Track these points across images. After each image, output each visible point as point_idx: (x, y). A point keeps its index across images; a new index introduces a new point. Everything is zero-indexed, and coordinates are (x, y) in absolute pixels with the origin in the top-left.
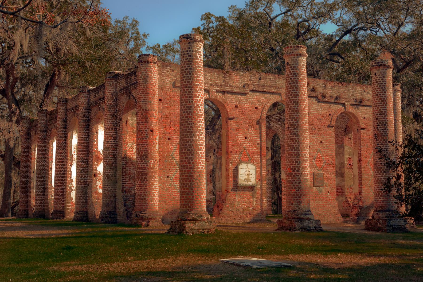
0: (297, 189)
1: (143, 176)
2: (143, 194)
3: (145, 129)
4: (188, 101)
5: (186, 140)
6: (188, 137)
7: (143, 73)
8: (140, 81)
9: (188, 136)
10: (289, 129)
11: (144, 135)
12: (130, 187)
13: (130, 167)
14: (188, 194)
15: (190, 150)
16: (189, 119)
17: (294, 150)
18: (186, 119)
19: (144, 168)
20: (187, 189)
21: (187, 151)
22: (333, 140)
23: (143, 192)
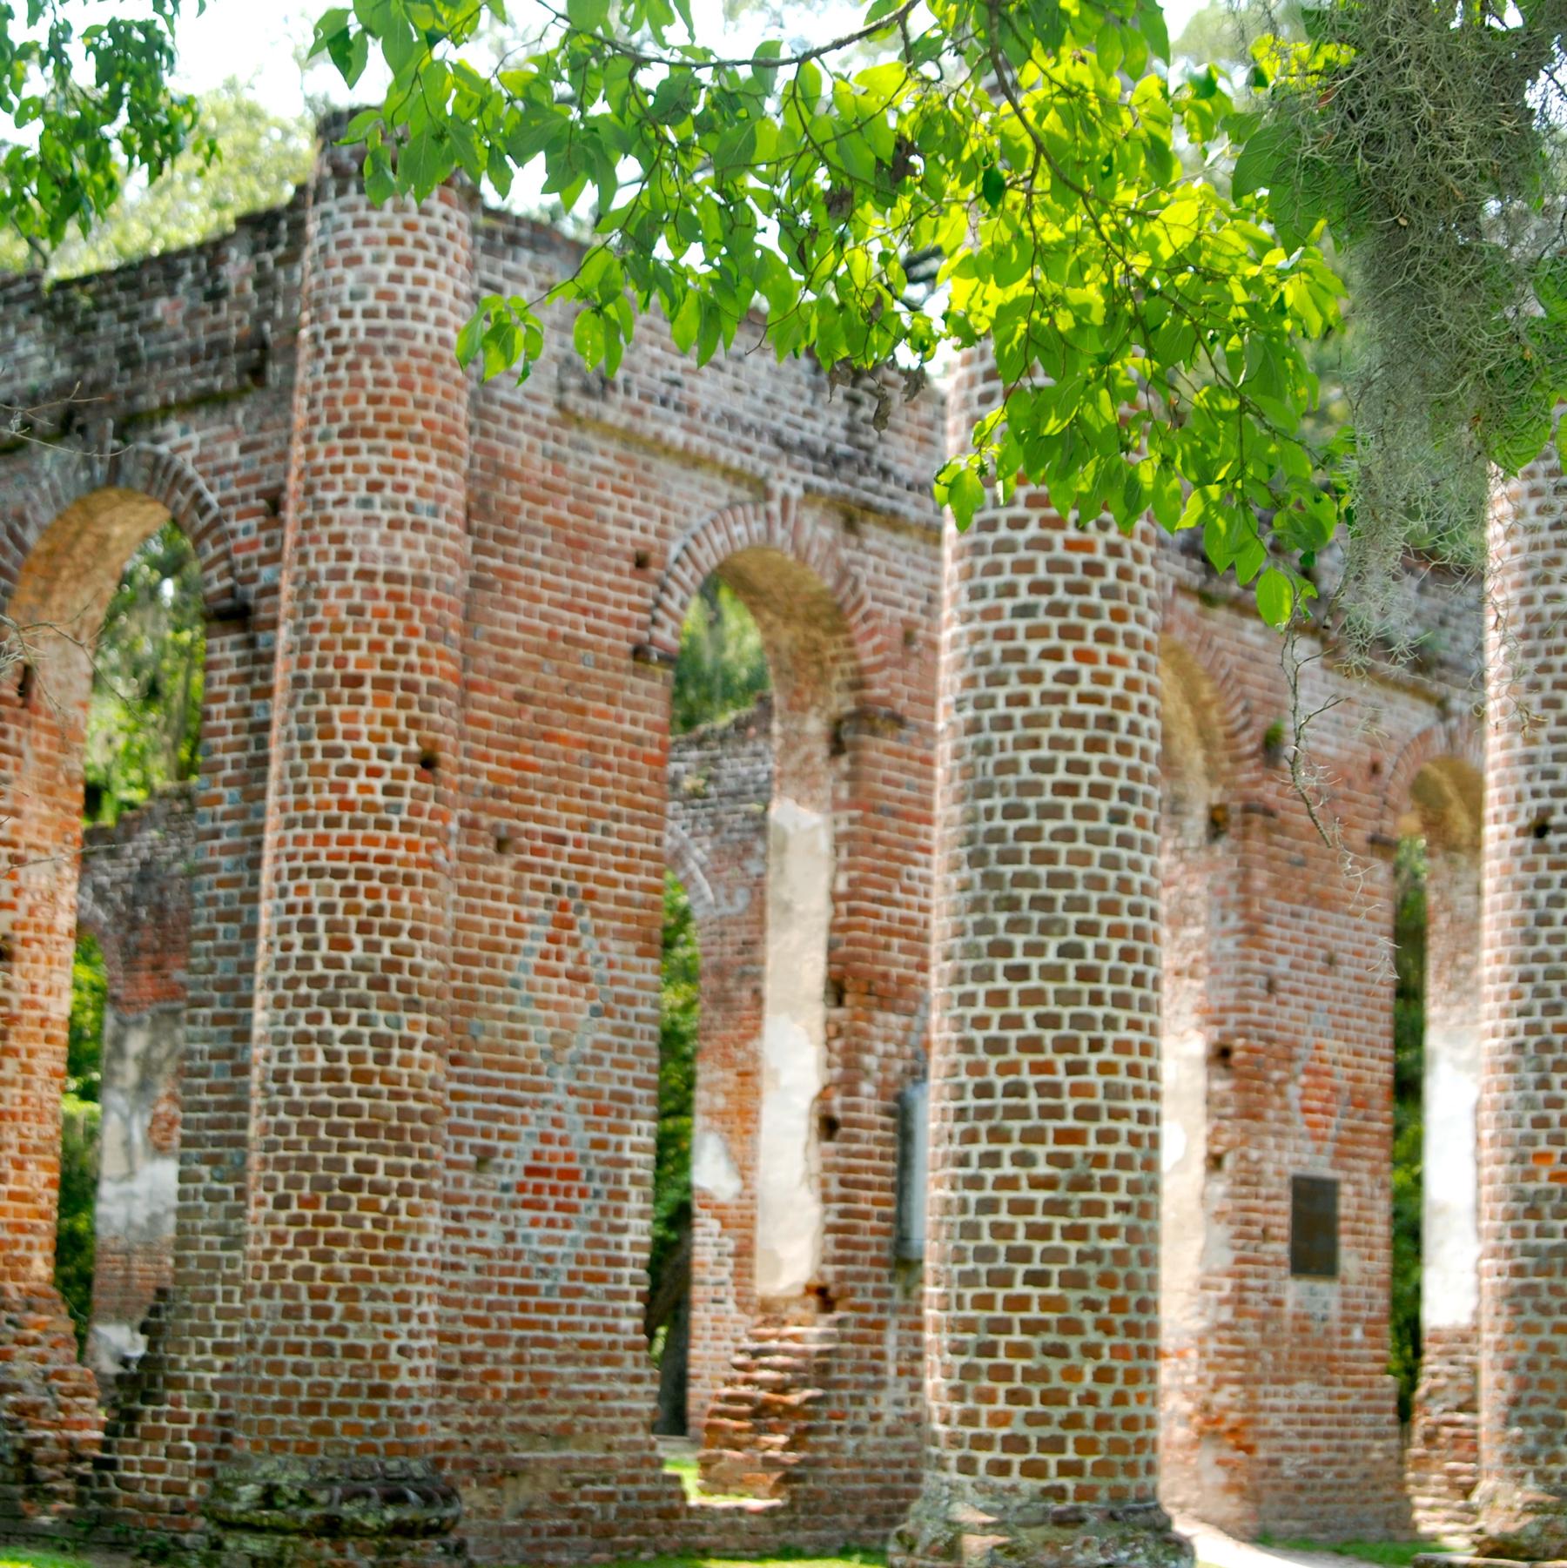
1: (343, 1147)
2: (339, 1308)
3: (374, 737)
7: (378, 259)
8: (345, 325)
11: (364, 789)
12: (20, 1228)
13: (31, 1054)
14: (1059, 1351)
16: (1071, 677)
18: (1050, 668)
19: (358, 1076)
21: (1051, 957)
23: (334, 1286)
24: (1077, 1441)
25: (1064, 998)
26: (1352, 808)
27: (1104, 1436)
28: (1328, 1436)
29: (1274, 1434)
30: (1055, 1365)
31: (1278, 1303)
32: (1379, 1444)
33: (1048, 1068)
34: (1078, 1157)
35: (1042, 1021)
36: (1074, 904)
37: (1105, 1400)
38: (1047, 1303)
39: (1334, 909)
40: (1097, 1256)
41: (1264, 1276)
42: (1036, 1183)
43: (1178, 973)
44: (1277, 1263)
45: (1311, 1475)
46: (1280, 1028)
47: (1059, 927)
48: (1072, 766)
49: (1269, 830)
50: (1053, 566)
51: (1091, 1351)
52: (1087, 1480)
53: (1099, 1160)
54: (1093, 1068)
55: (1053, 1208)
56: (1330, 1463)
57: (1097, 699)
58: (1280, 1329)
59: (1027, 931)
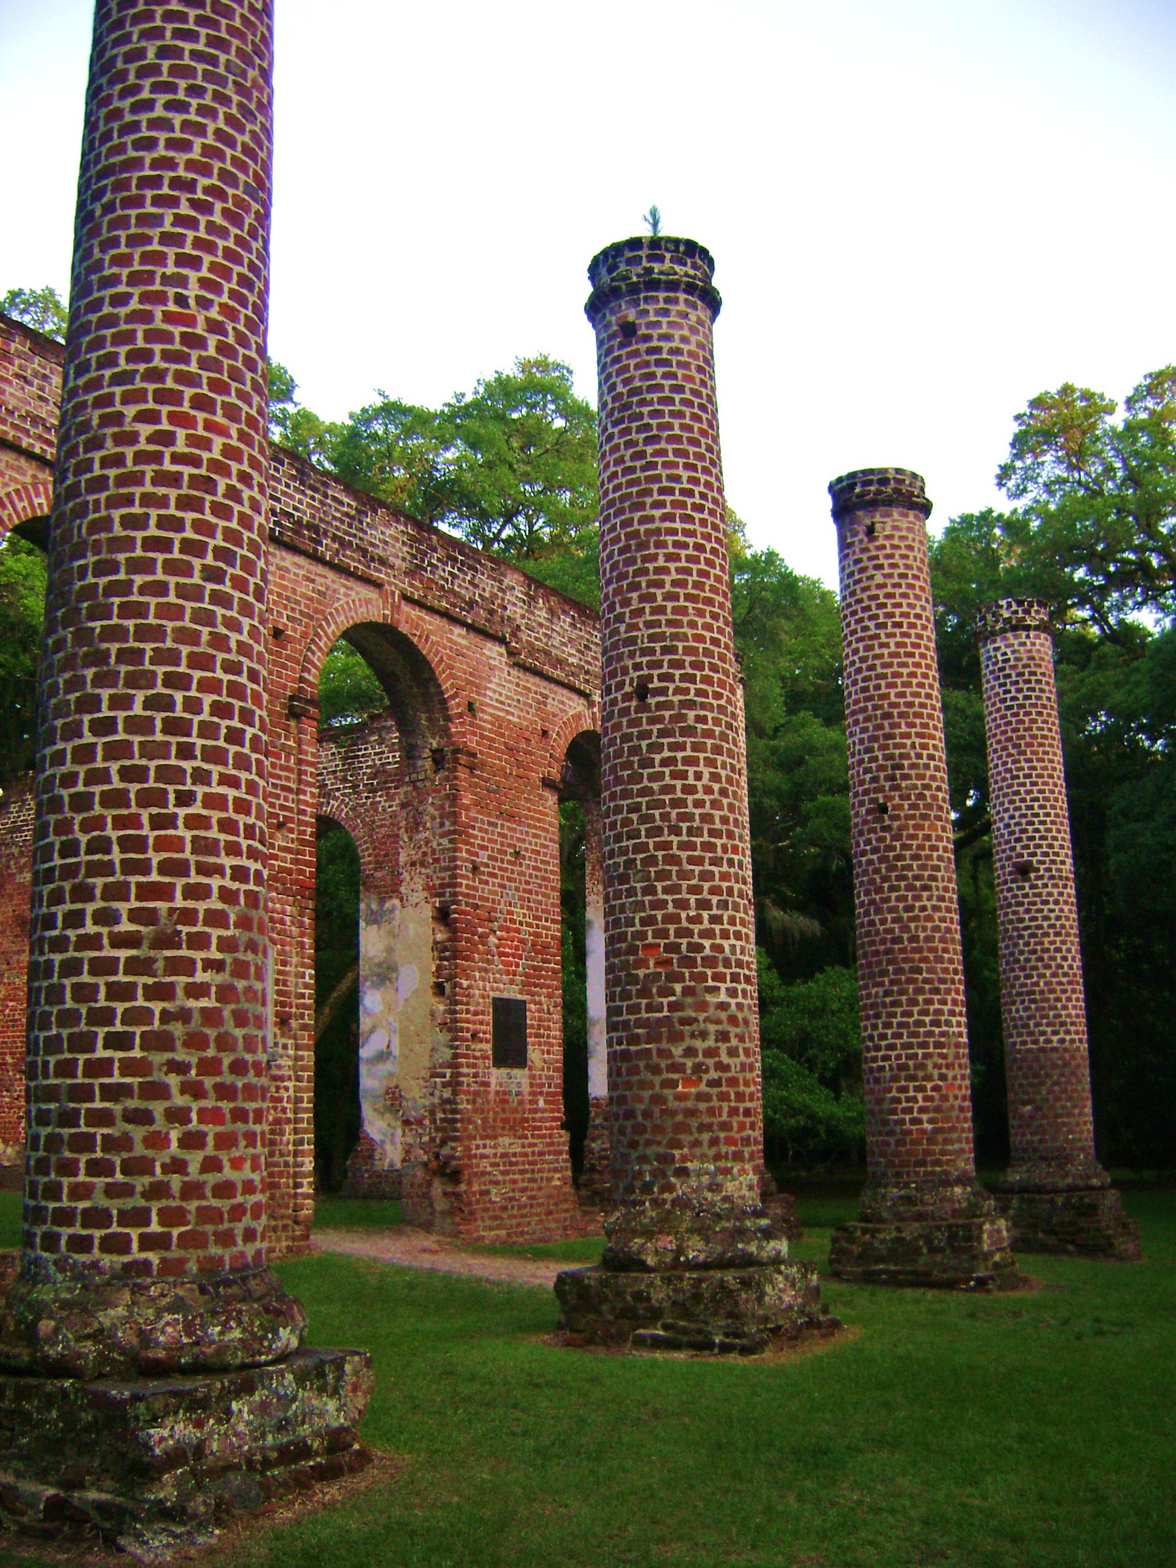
0: (713, 1075)
4: (171, 291)
5: (140, 611)
6: (160, 589)
9: (160, 576)
10: (652, 701)
14: (142, 1117)
15: (171, 706)
16: (167, 439)
17: (690, 831)
18: (145, 430)
20: (129, 1067)
22: (362, 949)
24: (161, 1212)
25: (150, 751)
26: (530, 758)
27: (192, 1206)
28: (522, 1172)
29: (483, 1173)
30: (138, 1133)
31: (487, 1084)
32: (558, 1175)
33: (134, 820)
34: (164, 913)
35: (127, 774)
36: (161, 657)
37: (193, 1168)
38: (129, 1067)
39: (520, 823)
40: (184, 1015)
41: (474, 1066)
42: (119, 941)
43: (413, 864)
44: (485, 1057)
45: (511, 1199)
46: (482, 898)
47: (149, 680)
48: (163, 522)
49: (471, 768)
50: (151, 336)
51: (178, 1116)
52: (175, 1253)
53: (188, 916)
54: (180, 822)
55: (134, 966)
56: (523, 1190)
57: (195, 462)
58: (488, 1102)
59: (114, 685)
